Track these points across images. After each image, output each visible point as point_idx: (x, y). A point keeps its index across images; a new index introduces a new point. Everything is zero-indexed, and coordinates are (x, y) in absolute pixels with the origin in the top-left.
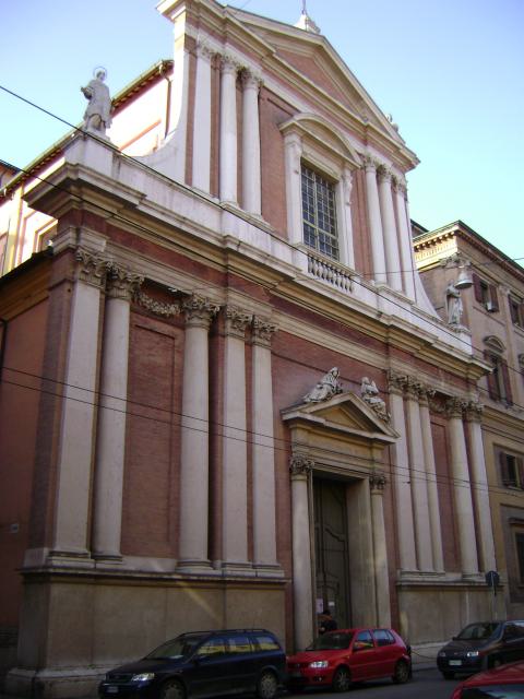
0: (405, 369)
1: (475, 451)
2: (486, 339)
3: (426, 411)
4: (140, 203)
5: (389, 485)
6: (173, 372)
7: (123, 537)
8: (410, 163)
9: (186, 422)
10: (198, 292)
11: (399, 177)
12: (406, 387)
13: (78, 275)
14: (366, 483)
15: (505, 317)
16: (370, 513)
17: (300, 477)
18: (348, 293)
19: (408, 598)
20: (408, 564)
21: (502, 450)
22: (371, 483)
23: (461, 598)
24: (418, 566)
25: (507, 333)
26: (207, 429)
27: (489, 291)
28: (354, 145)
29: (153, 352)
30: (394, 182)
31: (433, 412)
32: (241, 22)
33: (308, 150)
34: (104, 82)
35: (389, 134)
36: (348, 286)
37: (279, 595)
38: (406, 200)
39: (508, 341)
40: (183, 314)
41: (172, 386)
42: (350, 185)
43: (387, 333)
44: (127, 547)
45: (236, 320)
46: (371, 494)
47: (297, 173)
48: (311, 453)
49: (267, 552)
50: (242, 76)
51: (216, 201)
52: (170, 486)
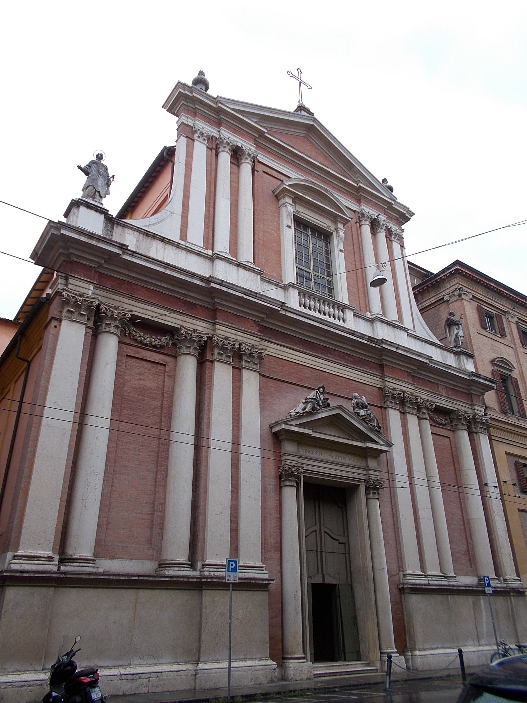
0: (404, 387)
1: (487, 461)
2: (492, 362)
3: (427, 424)
4: (123, 253)
5: (387, 490)
6: (163, 393)
7: (98, 543)
8: (403, 216)
9: (175, 437)
10: (185, 325)
11: (394, 227)
12: (403, 403)
13: (64, 313)
14: (362, 488)
15: (513, 339)
16: (370, 514)
17: (287, 483)
18: (341, 323)
19: (415, 602)
20: (412, 566)
21: (517, 459)
22: (367, 488)
23: (476, 606)
24: (423, 568)
25: (517, 355)
26: (192, 442)
27: (495, 319)
28: (345, 202)
29: (142, 377)
30: (389, 232)
31: (434, 424)
32: (232, 109)
33: (300, 209)
34: (102, 162)
35: (384, 196)
36: (341, 317)
37: (261, 597)
38: (402, 246)
39: (519, 362)
40: (174, 345)
41: (162, 404)
42: (342, 234)
43: (381, 356)
44: (101, 549)
45: (223, 348)
46: (367, 499)
47: (289, 227)
48: (301, 461)
49: (251, 556)
50: (237, 154)
51: (210, 252)
52: (155, 492)
